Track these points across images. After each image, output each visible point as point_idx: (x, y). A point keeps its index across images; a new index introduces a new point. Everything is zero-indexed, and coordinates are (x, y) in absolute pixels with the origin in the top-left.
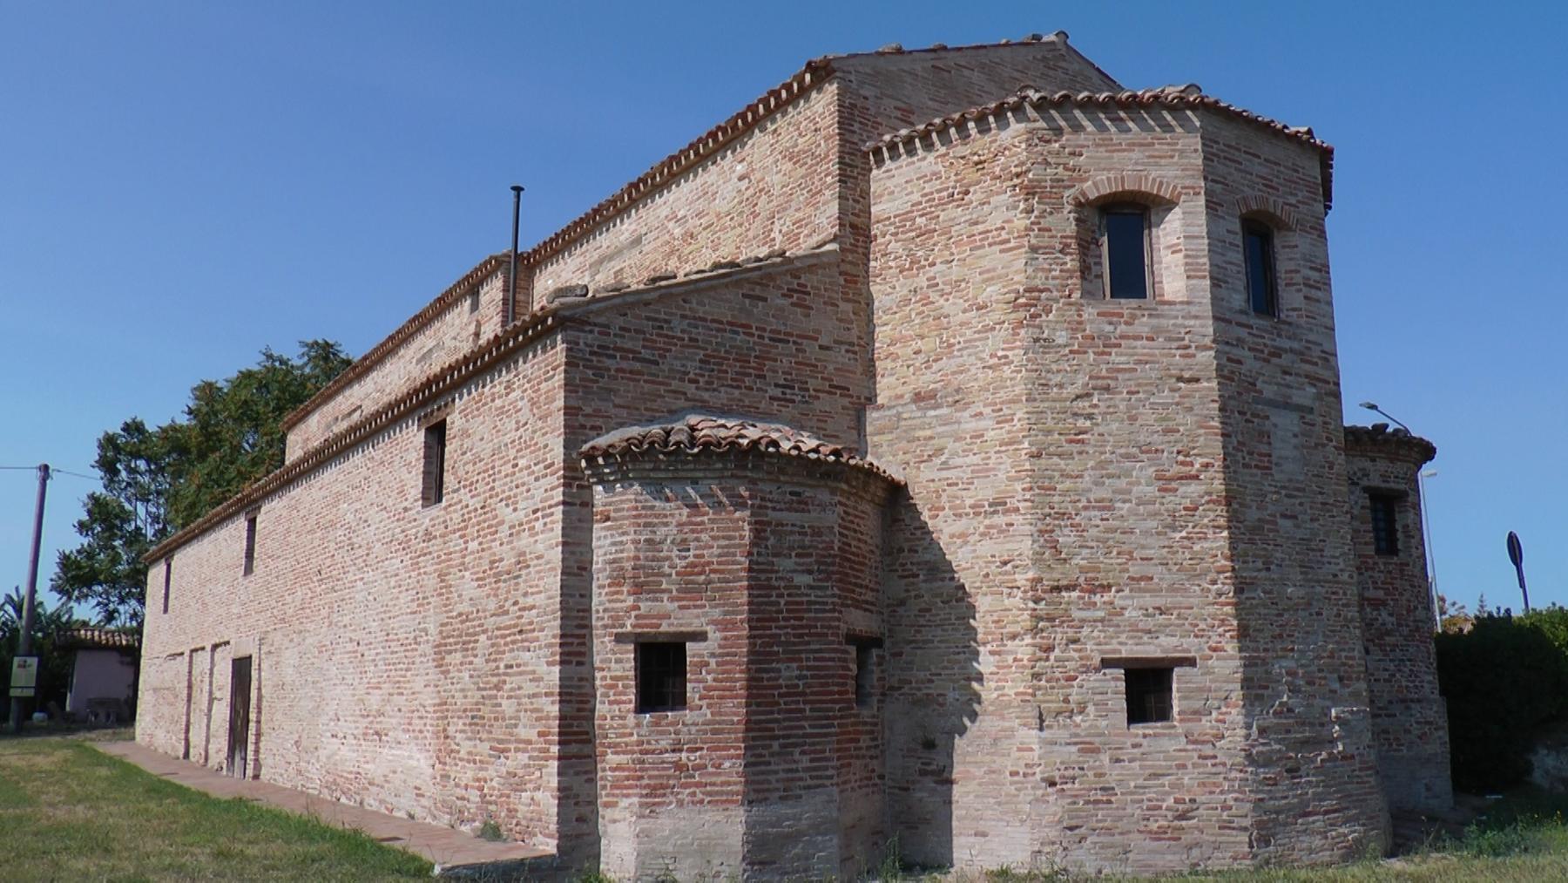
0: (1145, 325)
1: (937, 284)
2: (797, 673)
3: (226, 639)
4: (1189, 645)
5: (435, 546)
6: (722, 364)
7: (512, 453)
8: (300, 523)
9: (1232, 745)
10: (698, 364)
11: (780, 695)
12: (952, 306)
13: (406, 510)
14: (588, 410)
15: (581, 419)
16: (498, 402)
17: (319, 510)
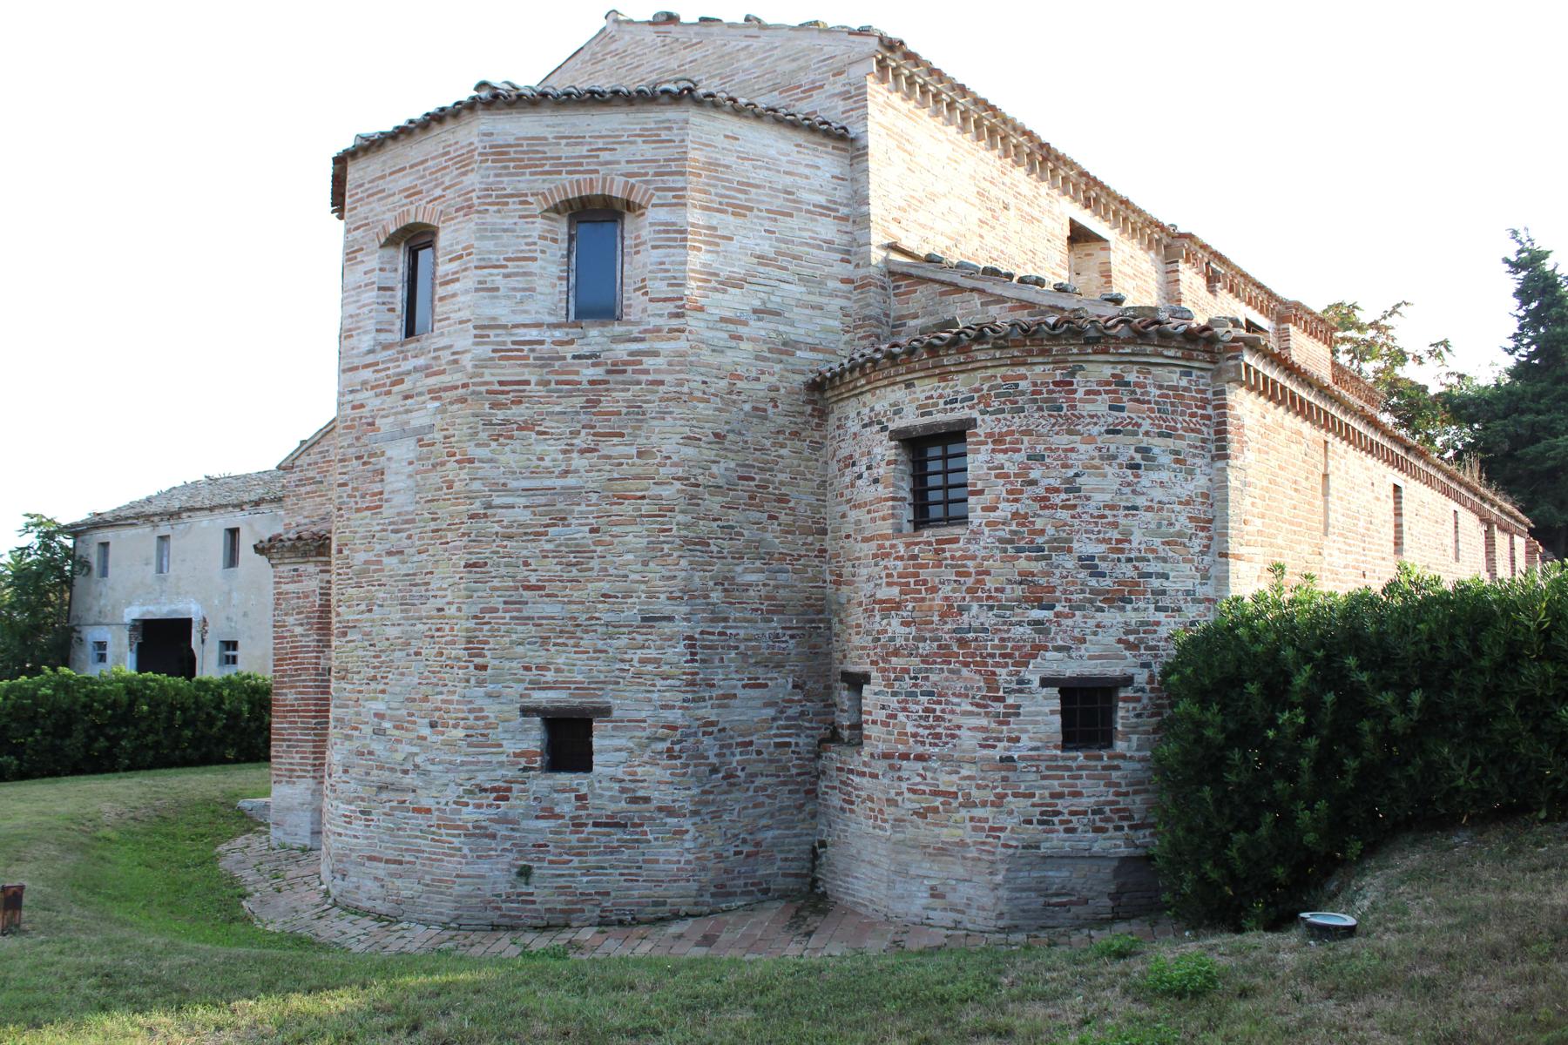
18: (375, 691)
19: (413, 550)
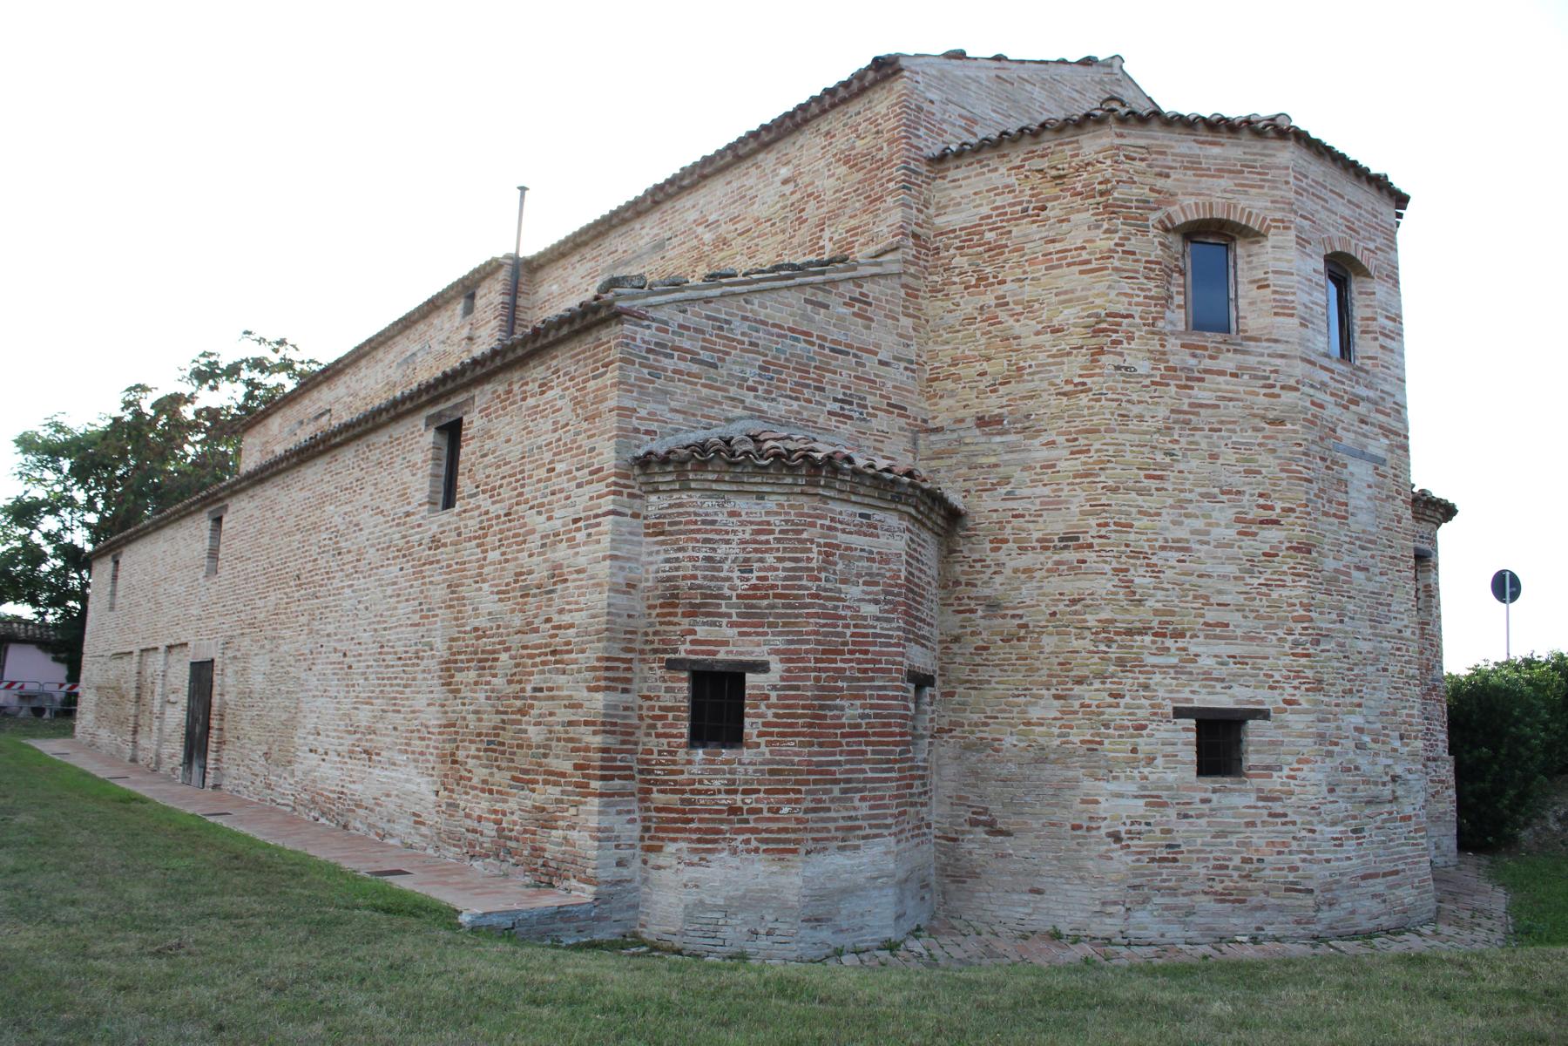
0: (1230, 360)
1: (1007, 304)
2: (861, 711)
3: (183, 640)
4: (1269, 699)
5: (444, 554)
6: (781, 373)
7: (548, 456)
8: (275, 524)
9: (1302, 803)
10: (757, 371)
11: (844, 735)
12: (1025, 329)
13: (408, 514)
14: (643, 413)
15: (635, 422)
16: (531, 401)
17: (298, 511)
18: (1352, 704)
19: (1377, 571)
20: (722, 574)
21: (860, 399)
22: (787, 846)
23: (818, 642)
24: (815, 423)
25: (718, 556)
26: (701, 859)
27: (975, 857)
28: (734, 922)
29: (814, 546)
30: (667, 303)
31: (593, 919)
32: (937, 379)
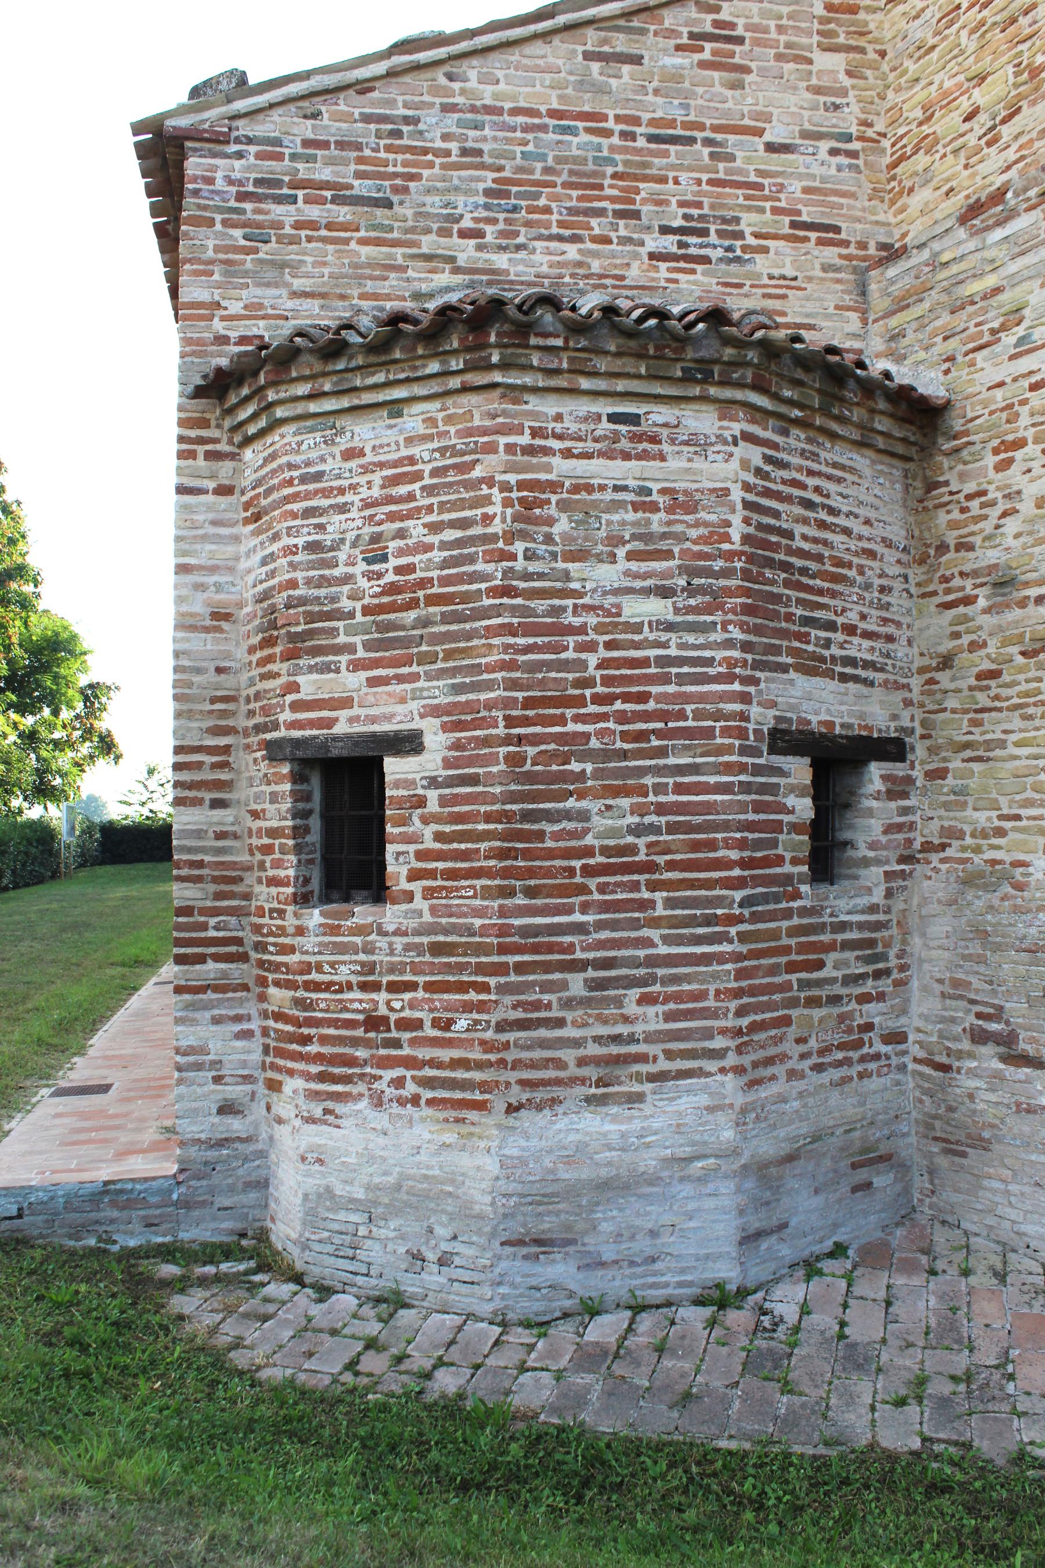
6: (537, 196)
10: (482, 200)
11: (588, 871)
14: (235, 308)
15: (218, 326)
20: (337, 572)
21: (725, 221)
22: (468, 1095)
23: (513, 685)
24: (622, 278)
25: (328, 539)
26: (327, 1111)
27: (981, 1106)
28: (383, 1233)
29: (495, 491)
30: (272, 106)
31: (176, 1204)
32: (903, 158)
